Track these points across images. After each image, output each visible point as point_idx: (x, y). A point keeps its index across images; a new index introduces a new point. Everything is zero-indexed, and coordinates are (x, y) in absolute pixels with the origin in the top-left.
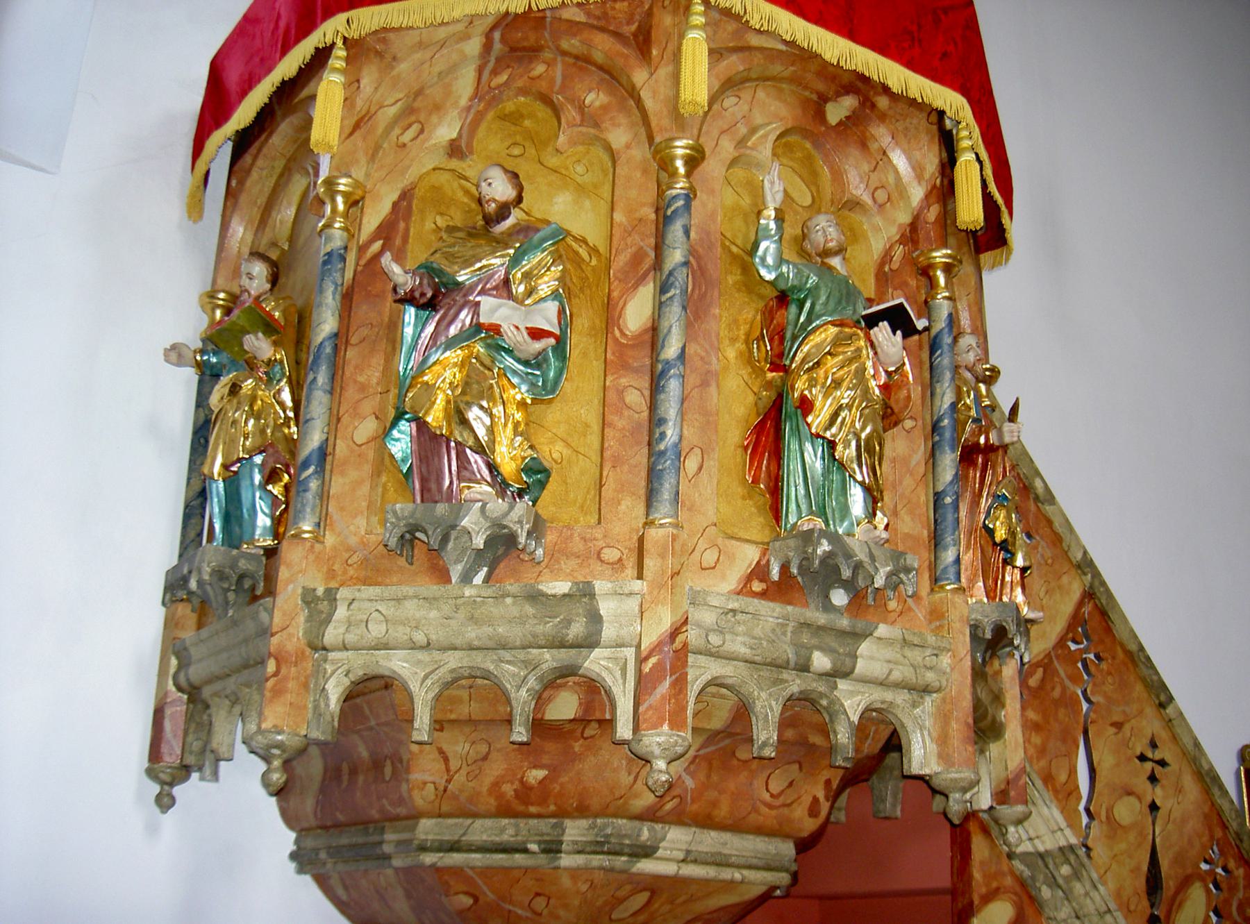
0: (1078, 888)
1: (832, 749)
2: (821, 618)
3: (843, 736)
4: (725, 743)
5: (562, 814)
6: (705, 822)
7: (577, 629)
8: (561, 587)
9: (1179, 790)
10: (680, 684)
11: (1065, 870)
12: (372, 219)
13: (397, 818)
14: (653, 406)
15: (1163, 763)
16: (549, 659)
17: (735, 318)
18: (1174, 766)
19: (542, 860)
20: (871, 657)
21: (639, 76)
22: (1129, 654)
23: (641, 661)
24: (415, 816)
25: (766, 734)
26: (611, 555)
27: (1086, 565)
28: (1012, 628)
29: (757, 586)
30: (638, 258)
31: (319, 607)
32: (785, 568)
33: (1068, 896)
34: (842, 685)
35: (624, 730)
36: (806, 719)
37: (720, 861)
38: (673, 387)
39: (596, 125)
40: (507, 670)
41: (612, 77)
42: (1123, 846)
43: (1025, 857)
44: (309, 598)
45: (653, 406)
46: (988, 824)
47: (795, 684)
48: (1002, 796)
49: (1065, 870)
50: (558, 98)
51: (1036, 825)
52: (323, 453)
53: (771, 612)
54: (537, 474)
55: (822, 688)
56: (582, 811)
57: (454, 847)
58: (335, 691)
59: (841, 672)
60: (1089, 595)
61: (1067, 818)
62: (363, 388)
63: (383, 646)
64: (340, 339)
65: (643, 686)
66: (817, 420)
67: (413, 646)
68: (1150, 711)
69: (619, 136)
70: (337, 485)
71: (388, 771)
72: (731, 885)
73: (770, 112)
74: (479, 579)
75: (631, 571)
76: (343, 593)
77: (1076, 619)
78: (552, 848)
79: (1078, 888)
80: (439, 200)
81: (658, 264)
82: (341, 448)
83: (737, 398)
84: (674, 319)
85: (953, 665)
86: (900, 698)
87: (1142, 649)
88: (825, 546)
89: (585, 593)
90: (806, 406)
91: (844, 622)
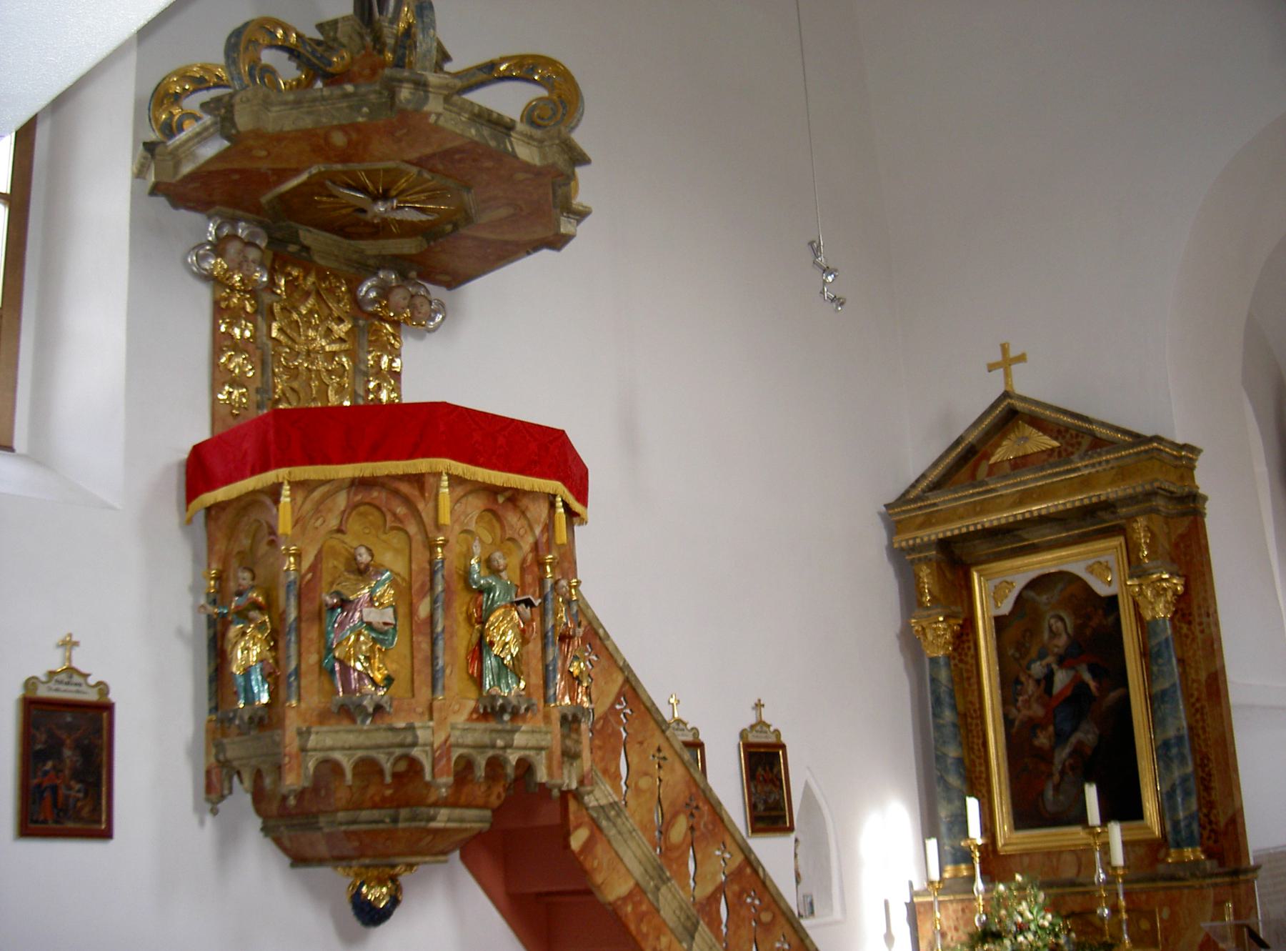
0: (619, 821)
1: (506, 775)
2: (500, 727)
3: (510, 771)
4: (464, 770)
5: (398, 807)
6: (455, 805)
7: (409, 740)
8: (402, 725)
9: (672, 770)
10: (449, 759)
11: (613, 813)
12: (306, 564)
13: (326, 812)
14: (433, 651)
15: (665, 758)
16: (398, 752)
17: (461, 604)
18: (670, 759)
19: (391, 826)
20: (519, 739)
21: (421, 506)
22: (647, 709)
23: (434, 752)
24: (337, 810)
25: (480, 772)
26: (420, 710)
27: (625, 669)
28: (580, 716)
29: (475, 716)
30: (423, 585)
31: (303, 734)
32: (485, 709)
33: (615, 825)
34: (509, 751)
35: (428, 777)
36: (495, 764)
37: (462, 820)
38: (440, 643)
39: (401, 522)
40: (381, 757)
41: (407, 501)
43: (594, 808)
44: (300, 733)
45: (433, 651)
46: (577, 795)
47: (490, 753)
48: (581, 783)
49: (613, 813)
50: (384, 509)
51: (597, 793)
52: (297, 671)
53: (481, 725)
54: (389, 680)
55: (500, 752)
56: (407, 805)
57: (354, 822)
58: (311, 765)
59: (509, 746)
60: (627, 680)
61: (613, 787)
62: (310, 640)
63: (332, 749)
64: (299, 619)
65: (434, 763)
66: (496, 650)
67: (343, 748)
68: (658, 733)
69: (412, 529)
70: (304, 682)
71: (323, 793)
72: (466, 830)
73: (476, 505)
74: (368, 722)
75: (427, 717)
76: (314, 729)
77: (620, 693)
78: (395, 820)
79: (619, 821)
80: (334, 553)
81: (432, 588)
82: (303, 667)
83: (463, 638)
84: (439, 614)
85: (553, 737)
86: (532, 753)
87: (653, 704)
88: (500, 701)
89: (411, 728)
90: (492, 644)
91: (508, 727)
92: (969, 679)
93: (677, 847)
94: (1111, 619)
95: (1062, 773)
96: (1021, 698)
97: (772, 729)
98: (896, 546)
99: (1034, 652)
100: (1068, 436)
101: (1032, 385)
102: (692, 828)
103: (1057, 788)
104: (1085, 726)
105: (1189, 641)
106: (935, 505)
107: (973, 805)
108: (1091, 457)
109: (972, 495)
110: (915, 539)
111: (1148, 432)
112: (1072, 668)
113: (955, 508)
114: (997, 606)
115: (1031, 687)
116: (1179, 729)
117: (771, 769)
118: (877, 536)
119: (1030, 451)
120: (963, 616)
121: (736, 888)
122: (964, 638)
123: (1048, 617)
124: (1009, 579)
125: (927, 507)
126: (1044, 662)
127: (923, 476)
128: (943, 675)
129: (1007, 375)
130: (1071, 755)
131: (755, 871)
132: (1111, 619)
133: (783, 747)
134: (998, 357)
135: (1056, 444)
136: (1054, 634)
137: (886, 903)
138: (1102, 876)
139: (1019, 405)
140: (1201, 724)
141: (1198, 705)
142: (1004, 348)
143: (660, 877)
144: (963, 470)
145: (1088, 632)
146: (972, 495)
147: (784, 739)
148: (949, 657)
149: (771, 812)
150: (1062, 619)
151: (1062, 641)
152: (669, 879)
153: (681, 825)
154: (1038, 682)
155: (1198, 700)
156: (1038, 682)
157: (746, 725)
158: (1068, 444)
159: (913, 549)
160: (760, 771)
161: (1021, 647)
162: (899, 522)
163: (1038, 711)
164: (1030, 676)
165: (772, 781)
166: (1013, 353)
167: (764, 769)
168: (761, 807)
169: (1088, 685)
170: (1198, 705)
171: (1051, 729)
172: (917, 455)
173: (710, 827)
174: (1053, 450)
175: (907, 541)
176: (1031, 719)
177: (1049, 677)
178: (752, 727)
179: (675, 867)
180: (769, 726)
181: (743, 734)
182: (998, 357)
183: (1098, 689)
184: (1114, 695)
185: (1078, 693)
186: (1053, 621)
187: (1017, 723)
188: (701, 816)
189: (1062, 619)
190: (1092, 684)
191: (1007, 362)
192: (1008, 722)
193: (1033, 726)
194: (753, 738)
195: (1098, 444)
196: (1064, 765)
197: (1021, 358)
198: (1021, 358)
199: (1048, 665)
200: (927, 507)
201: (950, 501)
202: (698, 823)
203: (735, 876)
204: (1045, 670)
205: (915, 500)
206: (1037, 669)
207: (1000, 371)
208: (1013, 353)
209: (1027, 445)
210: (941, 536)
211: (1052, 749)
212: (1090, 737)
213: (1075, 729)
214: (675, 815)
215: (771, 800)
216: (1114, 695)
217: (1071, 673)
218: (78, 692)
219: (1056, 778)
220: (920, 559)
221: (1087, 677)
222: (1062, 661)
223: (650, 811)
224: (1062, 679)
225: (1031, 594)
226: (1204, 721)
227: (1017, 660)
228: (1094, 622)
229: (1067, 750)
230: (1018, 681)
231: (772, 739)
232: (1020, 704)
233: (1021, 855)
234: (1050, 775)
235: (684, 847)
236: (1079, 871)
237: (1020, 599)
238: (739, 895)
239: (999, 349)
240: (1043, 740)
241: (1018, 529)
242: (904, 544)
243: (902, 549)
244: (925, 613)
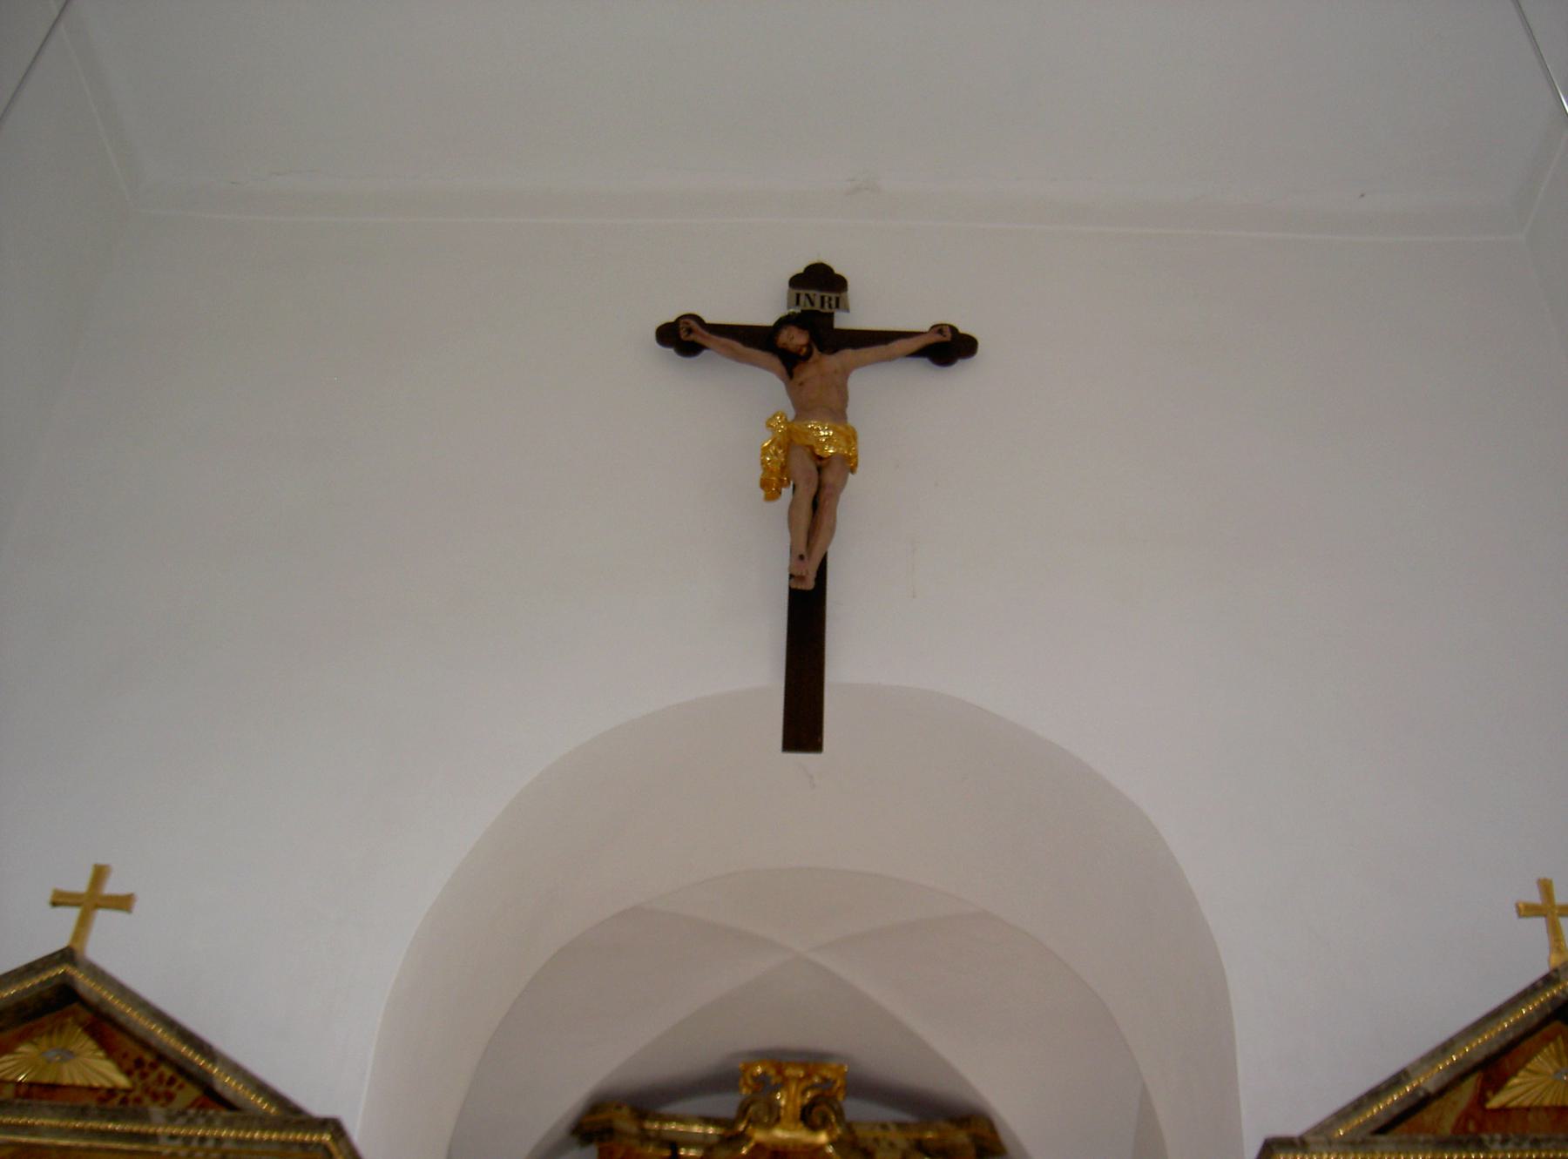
100: (153, 1076)
101: (126, 955)
108: (191, 1122)
111: (317, 1107)
119: (66, 1080)
129: (83, 924)
134: (80, 885)
135: (122, 1081)
137: (803, 726)
139: (84, 983)
142: (100, 874)
158: (146, 1090)
166: (111, 888)
174: (112, 1092)
182: (80, 885)
191: (94, 899)
195: (212, 1098)
197: (123, 903)
198: (123, 903)
207: (73, 914)
208: (111, 888)
209: (66, 1067)
239: (59, 910)
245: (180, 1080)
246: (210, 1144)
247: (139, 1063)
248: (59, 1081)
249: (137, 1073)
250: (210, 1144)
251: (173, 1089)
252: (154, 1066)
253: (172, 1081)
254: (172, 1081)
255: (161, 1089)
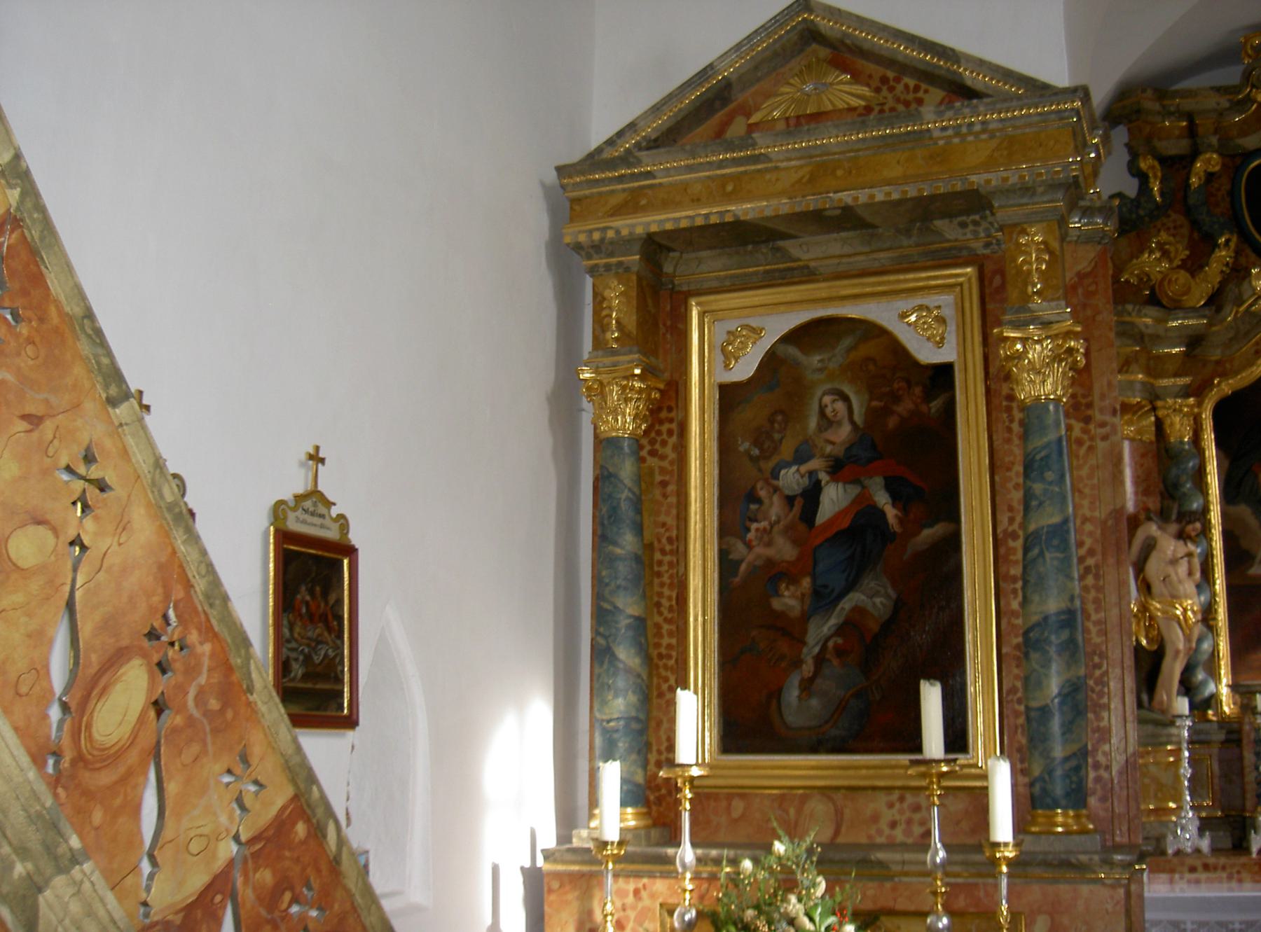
9: (123, 526)
15: (102, 486)
18: (119, 490)
42: (19, 598)
92: (664, 484)
93: (112, 756)
94: (936, 405)
95: (820, 660)
96: (754, 526)
97: (334, 512)
98: (567, 240)
99: (787, 450)
100: (900, 87)
102: (159, 707)
103: (807, 686)
104: (869, 583)
105: (1082, 451)
106: (649, 175)
107: (932, 698)
109: (721, 164)
110: (604, 229)
112: (856, 481)
113: (685, 186)
114: (726, 366)
115: (775, 509)
116: (1072, 599)
117: (325, 594)
118: (532, 225)
120: (667, 375)
121: (266, 876)
122: (664, 414)
123: (819, 393)
124: (754, 323)
125: (634, 177)
126: (804, 468)
127: (632, 126)
128: (627, 470)
130: (840, 630)
131: (317, 832)
132: (936, 405)
133: (351, 551)
136: (827, 422)
138: (942, 854)
139: (826, 25)
140: (1093, 593)
141: (1090, 562)
143: (49, 849)
144: (699, 130)
145: (892, 422)
146: (721, 164)
147: (355, 538)
148: (635, 440)
149: (318, 685)
150: (846, 399)
151: (843, 433)
152: (75, 860)
153: (131, 689)
154: (790, 500)
155: (1091, 552)
156: (790, 500)
157: (287, 495)
159: (597, 248)
160: (303, 595)
161: (764, 440)
162: (574, 201)
163: (784, 550)
164: (776, 489)
165: (324, 619)
167: (311, 592)
168: (298, 670)
169: (883, 514)
170: (1090, 562)
171: (806, 582)
172: (614, 101)
173: (214, 704)
175: (591, 232)
176: (770, 562)
177: (812, 494)
178: (299, 498)
179: (98, 816)
180: (330, 504)
181: (279, 510)
183: (901, 521)
184: (928, 534)
185: (862, 530)
186: (827, 399)
187: (743, 567)
188: (191, 671)
189: (846, 399)
190: (891, 513)
192: (727, 565)
193: (775, 575)
194: (294, 524)
195: (967, 93)
196: (824, 648)
199: (811, 473)
200: (634, 177)
201: (678, 170)
202: (182, 689)
203: (269, 843)
204: (806, 481)
205: (612, 164)
206: (791, 479)
210: (654, 228)
211: (805, 618)
212: (878, 600)
213: (850, 587)
214: (116, 659)
215: (317, 659)
216: (928, 534)
217: (854, 491)
218: (322, 526)
219: (808, 668)
220: (608, 267)
221: (882, 499)
222: (837, 468)
223: (40, 639)
224: (834, 499)
225: (792, 351)
226: (1099, 589)
227: (754, 460)
228: (904, 407)
229: (833, 621)
230: (753, 497)
231: (332, 534)
232: (751, 535)
233: (730, 797)
234: (797, 663)
235: (133, 757)
236: (837, 832)
237: (771, 361)
238: (270, 899)
240: (789, 600)
241: (785, 236)
242: (582, 238)
243: (578, 247)
244: (608, 360)
245: (924, 86)
246: (978, 128)
247: (884, 80)
248: (823, 109)
249: (885, 88)
250: (964, 130)
251: (920, 94)
252: (897, 80)
253: (917, 89)
254: (917, 89)
255: (910, 97)
